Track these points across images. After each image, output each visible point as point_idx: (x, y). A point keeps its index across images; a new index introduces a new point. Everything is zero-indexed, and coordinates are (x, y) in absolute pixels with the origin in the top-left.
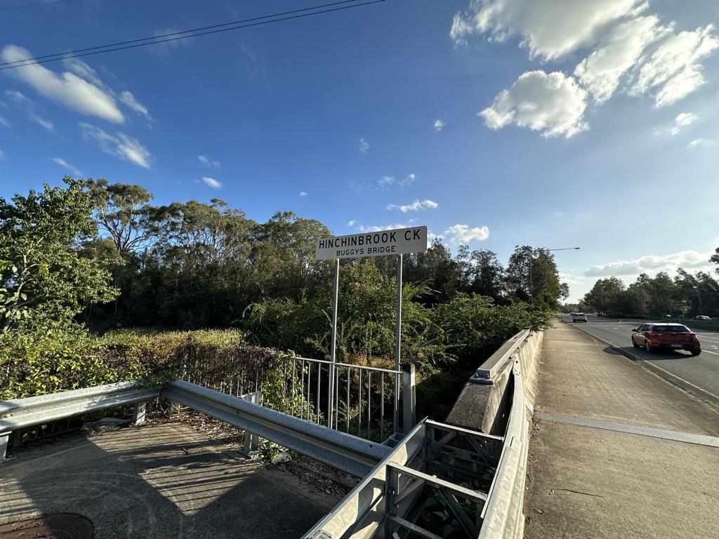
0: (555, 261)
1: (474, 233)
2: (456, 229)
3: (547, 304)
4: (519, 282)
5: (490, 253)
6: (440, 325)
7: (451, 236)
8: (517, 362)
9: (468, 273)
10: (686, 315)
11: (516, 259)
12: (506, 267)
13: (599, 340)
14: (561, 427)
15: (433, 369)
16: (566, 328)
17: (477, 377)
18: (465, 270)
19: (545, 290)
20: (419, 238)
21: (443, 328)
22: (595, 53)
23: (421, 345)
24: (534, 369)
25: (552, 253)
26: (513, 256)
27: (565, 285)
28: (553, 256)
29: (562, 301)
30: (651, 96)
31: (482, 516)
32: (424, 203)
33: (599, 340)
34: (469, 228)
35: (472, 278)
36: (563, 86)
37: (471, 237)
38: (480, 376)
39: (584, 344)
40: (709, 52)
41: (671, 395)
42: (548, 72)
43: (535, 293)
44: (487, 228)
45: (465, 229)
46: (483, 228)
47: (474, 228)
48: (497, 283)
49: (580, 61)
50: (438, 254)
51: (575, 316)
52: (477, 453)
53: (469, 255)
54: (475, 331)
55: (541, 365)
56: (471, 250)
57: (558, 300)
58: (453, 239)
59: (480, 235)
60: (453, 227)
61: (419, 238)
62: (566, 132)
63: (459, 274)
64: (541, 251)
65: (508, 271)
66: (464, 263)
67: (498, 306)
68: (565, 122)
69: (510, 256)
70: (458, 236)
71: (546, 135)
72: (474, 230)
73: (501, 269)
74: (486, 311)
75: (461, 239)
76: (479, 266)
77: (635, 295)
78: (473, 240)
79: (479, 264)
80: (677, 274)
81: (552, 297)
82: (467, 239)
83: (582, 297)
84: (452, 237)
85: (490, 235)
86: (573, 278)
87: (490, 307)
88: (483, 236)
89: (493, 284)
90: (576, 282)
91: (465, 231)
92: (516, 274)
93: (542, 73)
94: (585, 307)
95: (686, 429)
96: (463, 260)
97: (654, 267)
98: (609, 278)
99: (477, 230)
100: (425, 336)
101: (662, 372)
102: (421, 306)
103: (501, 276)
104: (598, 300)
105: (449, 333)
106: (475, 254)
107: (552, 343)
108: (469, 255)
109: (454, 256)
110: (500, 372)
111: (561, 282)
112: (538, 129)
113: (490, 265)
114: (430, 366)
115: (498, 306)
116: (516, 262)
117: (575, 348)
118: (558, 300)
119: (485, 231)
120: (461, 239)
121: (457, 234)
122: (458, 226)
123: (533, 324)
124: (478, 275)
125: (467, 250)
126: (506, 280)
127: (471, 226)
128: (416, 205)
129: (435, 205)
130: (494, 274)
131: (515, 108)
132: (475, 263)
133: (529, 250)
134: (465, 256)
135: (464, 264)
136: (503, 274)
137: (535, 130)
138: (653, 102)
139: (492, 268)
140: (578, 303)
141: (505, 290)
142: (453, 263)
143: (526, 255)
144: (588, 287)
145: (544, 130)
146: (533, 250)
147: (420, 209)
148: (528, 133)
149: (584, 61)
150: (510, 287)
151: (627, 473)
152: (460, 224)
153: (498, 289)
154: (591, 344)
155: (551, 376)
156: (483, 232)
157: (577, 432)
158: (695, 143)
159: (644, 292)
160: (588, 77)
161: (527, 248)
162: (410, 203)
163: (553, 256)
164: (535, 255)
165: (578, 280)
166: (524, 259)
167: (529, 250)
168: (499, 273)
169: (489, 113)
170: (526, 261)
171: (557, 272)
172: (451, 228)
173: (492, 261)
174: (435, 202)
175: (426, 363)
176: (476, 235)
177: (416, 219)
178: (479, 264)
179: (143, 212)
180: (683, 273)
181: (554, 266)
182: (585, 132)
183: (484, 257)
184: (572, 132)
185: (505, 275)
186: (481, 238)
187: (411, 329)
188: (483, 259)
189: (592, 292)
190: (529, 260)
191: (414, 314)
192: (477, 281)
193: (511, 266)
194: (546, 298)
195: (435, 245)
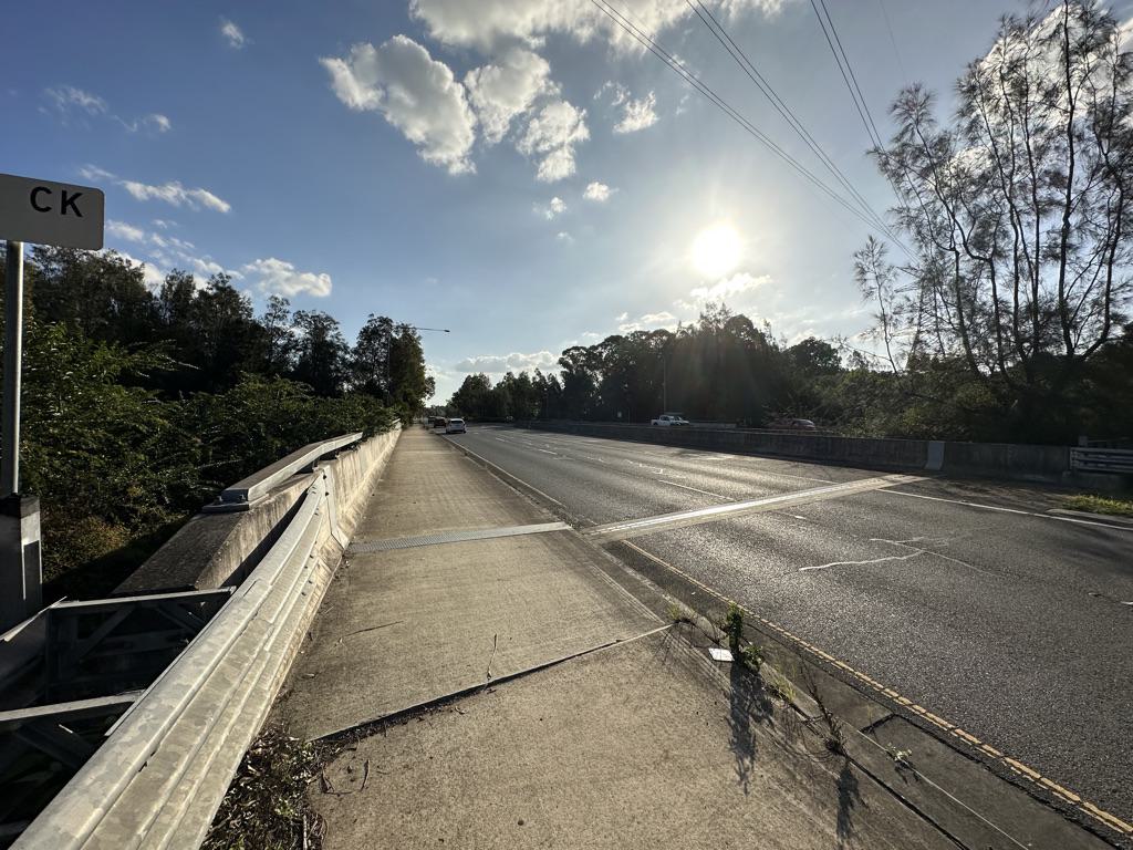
0: (422, 345)
1: (306, 282)
2: (269, 267)
3: (407, 404)
4: (372, 372)
5: (328, 319)
6: (196, 431)
7: (255, 277)
8: (325, 477)
9: (286, 349)
10: (538, 417)
11: (369, 335)
12: (353, 344)
13: (457, 447)
14: (380, 555)
15: (168, 514)
16: (424, 435)
17: (220, 503)
18: (281, 342)
19: (406, 384)
20: (79, 214)
21: (202, 437)
22: (489, 67)
23: (138, 470)
24: (366, 489)
25: (418, 333)
26: (365, 330)
27: (431, 379)
28: (420, 338)
29: (428, 403)
30: (534, 162)
31: (107, 734)
32: (195, 193)
33: (457, 447)
34: (295, 271)
35: (295, 357)
36: (451, 89)
37: (300, 288)
38: (225, 501)
39: (440, 453)
40: (548, 106)
41: (503, 494)
42: (434, 58)
43: (392, 387)
44: (328, 279)
45: (287, 270)
46: (322, 276)
47: (306, 272)
48: (337, 370)
49: (473, 69)
50: (222, 304)
51: (436, 422)
52: (179, 627)
53: (290, 316)
54: (270, 439)
55: (380, 484)
56: (292, 309)
57: (423, 399)
58: (263, 284)
59: (316, 286)
60: (263, 260)
61: (79, 214)
62: (450, 162)
63: (269, 348)
64: (405, 328)
65: (355, 352)
66: (279, 329)
67: (319, 398)
68: (449, 148)
69: (360, 329)
70: (271, 280)
71: (426, 156)
72: (304, 276)
73: (345, 349)
74: (293, 405)
75: (278, 287)
76: (308, 339)
77: (499, 395)
78: (301, 294)
79: (308, 336)
80: (534, 375)
81: (414, 395)
82: (291, 290)
83: (450, 397)
84: (259, 281)
85: (334, 290)
86: (442, 373)
87: (305, 401)
88: (321, 290)
89: (331, 371)
90: (446, 378)
91: (287, 274)
92: (367, 358)
93: (426, 54)
94: (452, 410)
95: (503, 524)
96: (278, 324)
97: (518, 366)
98: (478, 374)
99: (310, 277)
100: (151, 454)
101: (503, 473)
102: (151, 396)
103: (343, 359)
104: (465, 401)
105: (214, 444)
106: (300, 318)
107: (403, 455)
108: (290, 316)
109: (259, 313)
110: (275, 489)
111: (426, 376)
112: (416, 142)
113: (328, 339)
114: (158, 510)
115: (319, 398)
116: (369, 340)
117: (429, 458)
118: (423, 399)
119: (324, 281)
120: (278, 287)
121: (271, 276)
122: (272, 261)
123: (369, 423)
124: (305, 354)
125: (286, 307)
126: (351, 365)
127: (301, 268)
128: (172, 192)
129: (225, 207)
130: (334, 355)
131: (384, 88)
132: (300, 333)
133: (387, 323)
134: (280, 318)
135: (280, 333)
136: (347, 356)
137: (411, 141)
138: (536, 171)
139: (331, 344)
140: (445, 405)
141: (349, 381)
142: (256, 326)
143: (384, 330)
144: (457, 386)
145: (422, 146)
146: (394, 324)
147: (184, 204)
148: (396, 137)
149: (478, 70)
150: (357, 378)
151: (438, 585)
152: (277, 258)
153: (338, 380)
154: (447, 452)
155: (388, 495)
156: (321, 283)
157: (397, 557)
158: (561, 235)
159: (507, 393)
160: (480, 97)
161: (386, 321)
162: (159, 182)
163: (420, 338)
164: (397, 332)
165: (449, 376)
166: (381, 336)
167: (387, 323)
168: (340, 353)
169: (338, 67)
170: (383, 340)
171: (423, 361)
172: (259, 261)
173: (331, 333)
174: (222, 198)
175: (152, 505)
176: (308, 287)
177: (174, 224)
178: (308, 336)
179: (336, 506)
180: (539, 374)
181: (420, 351)
182: (470, 175)
183: (319, 326)
184: (457, 168)
185: (350, 358)
186: (317, 293)
187: (108, 440)
188: (316, 328)
189: (460, 390)
190: (387, 339)
191: (123, 410)
192: (304, 361)
193: (360, 344)
194: (406, 396)
195: (216, 286)
